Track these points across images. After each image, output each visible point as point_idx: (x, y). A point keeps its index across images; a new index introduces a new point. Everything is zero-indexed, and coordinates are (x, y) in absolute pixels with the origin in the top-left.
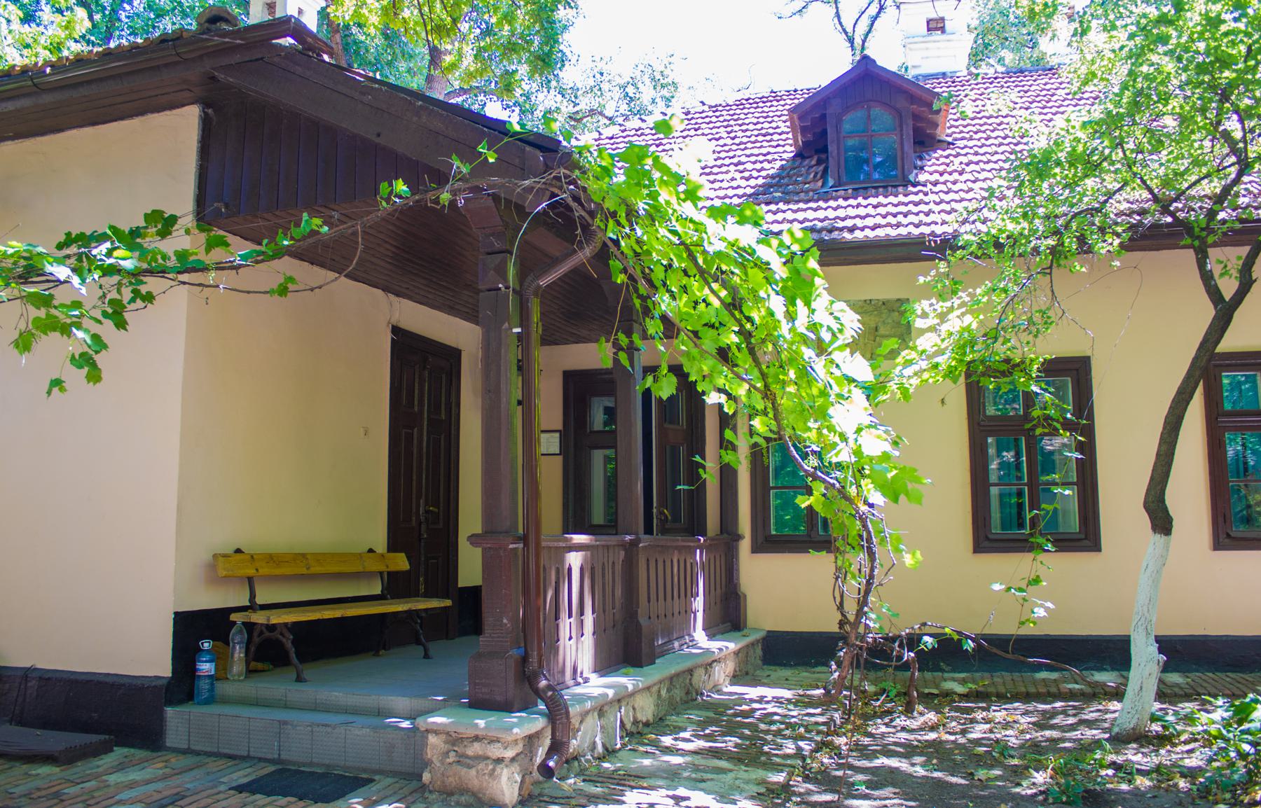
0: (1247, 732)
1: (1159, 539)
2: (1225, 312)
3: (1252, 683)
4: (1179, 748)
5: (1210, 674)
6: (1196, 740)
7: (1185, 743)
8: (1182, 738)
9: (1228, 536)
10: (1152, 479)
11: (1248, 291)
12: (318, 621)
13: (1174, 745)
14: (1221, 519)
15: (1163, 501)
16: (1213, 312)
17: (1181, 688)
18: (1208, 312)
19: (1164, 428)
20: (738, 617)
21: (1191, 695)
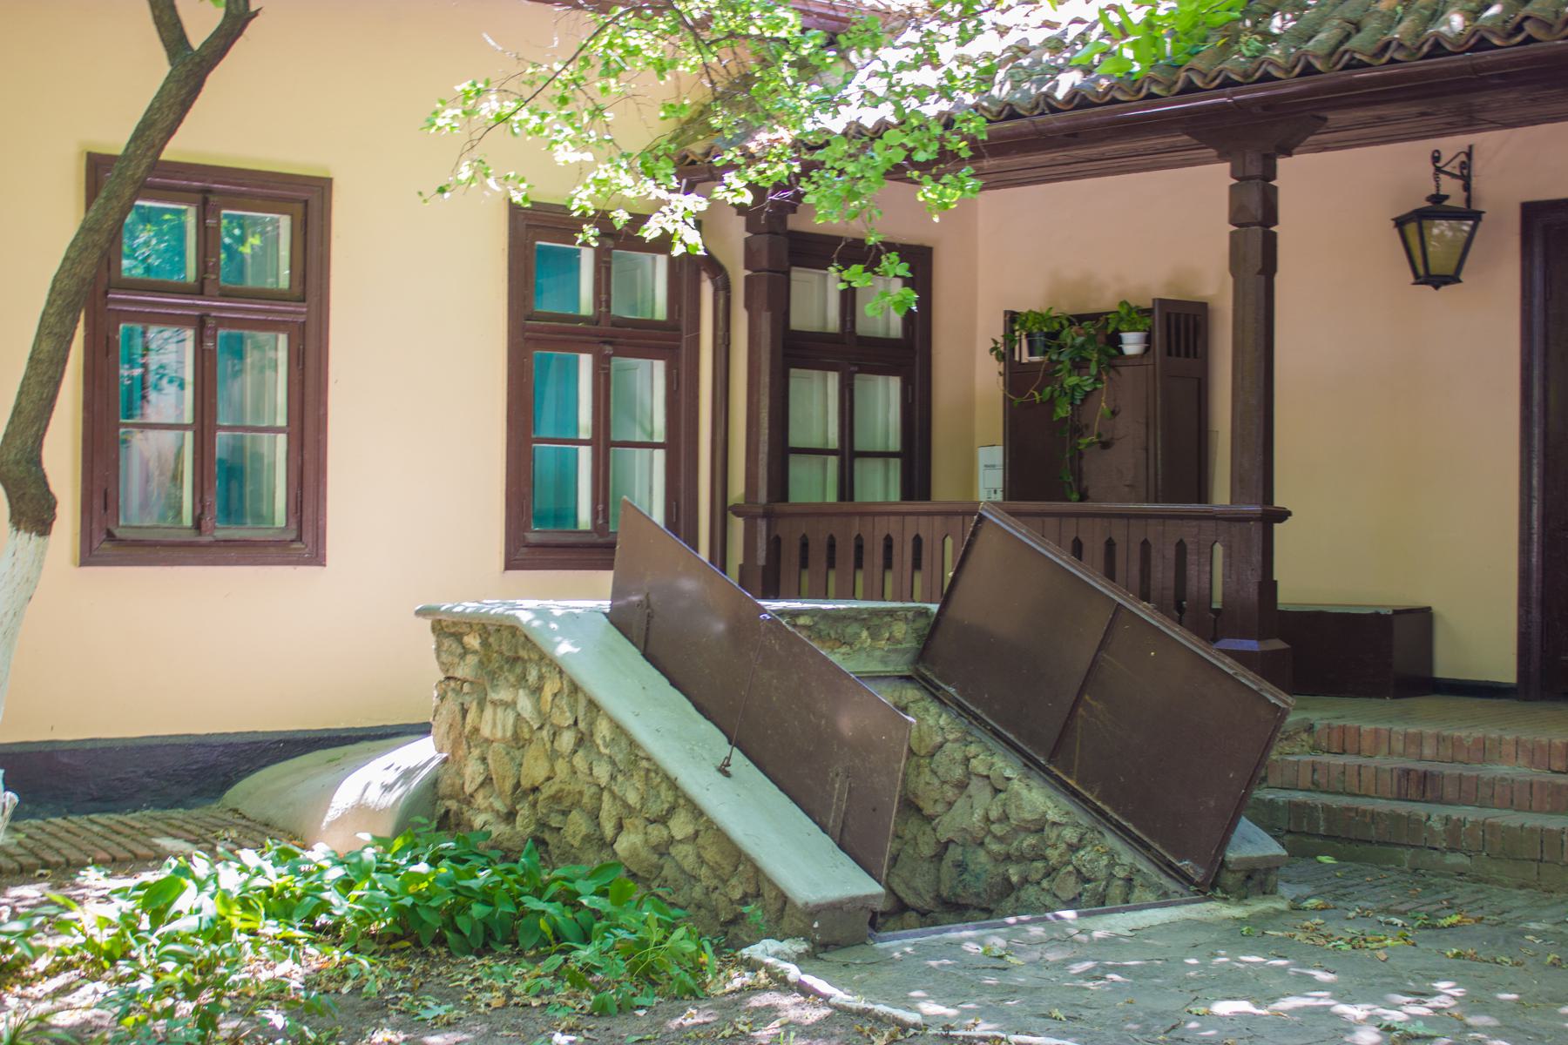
0: (171, 938)
1: (26, 542)
2: (190, 71)
3: (143, 831)
4: (33, 991)
5: (58, 821)
6: (69, 966)
7: (48, 974)
8: (42, 964)
9: (110, 536)
10: (17, 411)
11: (240, 33)
12: (771, 420)
13: (28, 982)
14: (98, 502)
15: (39, 463)
16: (167, 69)
17: (10, 856)
18: (157, 68)
19: (50, 303)
20: (286, 742)
21: (32, 869)
